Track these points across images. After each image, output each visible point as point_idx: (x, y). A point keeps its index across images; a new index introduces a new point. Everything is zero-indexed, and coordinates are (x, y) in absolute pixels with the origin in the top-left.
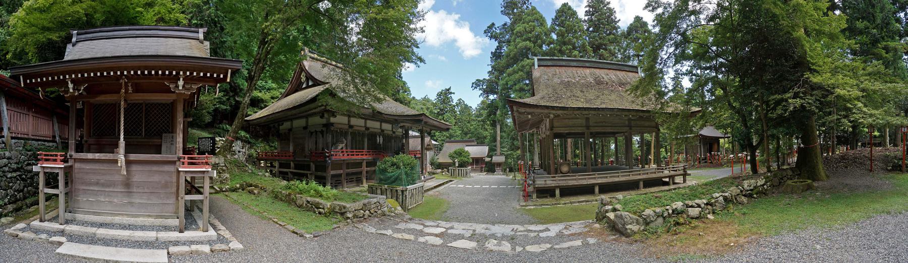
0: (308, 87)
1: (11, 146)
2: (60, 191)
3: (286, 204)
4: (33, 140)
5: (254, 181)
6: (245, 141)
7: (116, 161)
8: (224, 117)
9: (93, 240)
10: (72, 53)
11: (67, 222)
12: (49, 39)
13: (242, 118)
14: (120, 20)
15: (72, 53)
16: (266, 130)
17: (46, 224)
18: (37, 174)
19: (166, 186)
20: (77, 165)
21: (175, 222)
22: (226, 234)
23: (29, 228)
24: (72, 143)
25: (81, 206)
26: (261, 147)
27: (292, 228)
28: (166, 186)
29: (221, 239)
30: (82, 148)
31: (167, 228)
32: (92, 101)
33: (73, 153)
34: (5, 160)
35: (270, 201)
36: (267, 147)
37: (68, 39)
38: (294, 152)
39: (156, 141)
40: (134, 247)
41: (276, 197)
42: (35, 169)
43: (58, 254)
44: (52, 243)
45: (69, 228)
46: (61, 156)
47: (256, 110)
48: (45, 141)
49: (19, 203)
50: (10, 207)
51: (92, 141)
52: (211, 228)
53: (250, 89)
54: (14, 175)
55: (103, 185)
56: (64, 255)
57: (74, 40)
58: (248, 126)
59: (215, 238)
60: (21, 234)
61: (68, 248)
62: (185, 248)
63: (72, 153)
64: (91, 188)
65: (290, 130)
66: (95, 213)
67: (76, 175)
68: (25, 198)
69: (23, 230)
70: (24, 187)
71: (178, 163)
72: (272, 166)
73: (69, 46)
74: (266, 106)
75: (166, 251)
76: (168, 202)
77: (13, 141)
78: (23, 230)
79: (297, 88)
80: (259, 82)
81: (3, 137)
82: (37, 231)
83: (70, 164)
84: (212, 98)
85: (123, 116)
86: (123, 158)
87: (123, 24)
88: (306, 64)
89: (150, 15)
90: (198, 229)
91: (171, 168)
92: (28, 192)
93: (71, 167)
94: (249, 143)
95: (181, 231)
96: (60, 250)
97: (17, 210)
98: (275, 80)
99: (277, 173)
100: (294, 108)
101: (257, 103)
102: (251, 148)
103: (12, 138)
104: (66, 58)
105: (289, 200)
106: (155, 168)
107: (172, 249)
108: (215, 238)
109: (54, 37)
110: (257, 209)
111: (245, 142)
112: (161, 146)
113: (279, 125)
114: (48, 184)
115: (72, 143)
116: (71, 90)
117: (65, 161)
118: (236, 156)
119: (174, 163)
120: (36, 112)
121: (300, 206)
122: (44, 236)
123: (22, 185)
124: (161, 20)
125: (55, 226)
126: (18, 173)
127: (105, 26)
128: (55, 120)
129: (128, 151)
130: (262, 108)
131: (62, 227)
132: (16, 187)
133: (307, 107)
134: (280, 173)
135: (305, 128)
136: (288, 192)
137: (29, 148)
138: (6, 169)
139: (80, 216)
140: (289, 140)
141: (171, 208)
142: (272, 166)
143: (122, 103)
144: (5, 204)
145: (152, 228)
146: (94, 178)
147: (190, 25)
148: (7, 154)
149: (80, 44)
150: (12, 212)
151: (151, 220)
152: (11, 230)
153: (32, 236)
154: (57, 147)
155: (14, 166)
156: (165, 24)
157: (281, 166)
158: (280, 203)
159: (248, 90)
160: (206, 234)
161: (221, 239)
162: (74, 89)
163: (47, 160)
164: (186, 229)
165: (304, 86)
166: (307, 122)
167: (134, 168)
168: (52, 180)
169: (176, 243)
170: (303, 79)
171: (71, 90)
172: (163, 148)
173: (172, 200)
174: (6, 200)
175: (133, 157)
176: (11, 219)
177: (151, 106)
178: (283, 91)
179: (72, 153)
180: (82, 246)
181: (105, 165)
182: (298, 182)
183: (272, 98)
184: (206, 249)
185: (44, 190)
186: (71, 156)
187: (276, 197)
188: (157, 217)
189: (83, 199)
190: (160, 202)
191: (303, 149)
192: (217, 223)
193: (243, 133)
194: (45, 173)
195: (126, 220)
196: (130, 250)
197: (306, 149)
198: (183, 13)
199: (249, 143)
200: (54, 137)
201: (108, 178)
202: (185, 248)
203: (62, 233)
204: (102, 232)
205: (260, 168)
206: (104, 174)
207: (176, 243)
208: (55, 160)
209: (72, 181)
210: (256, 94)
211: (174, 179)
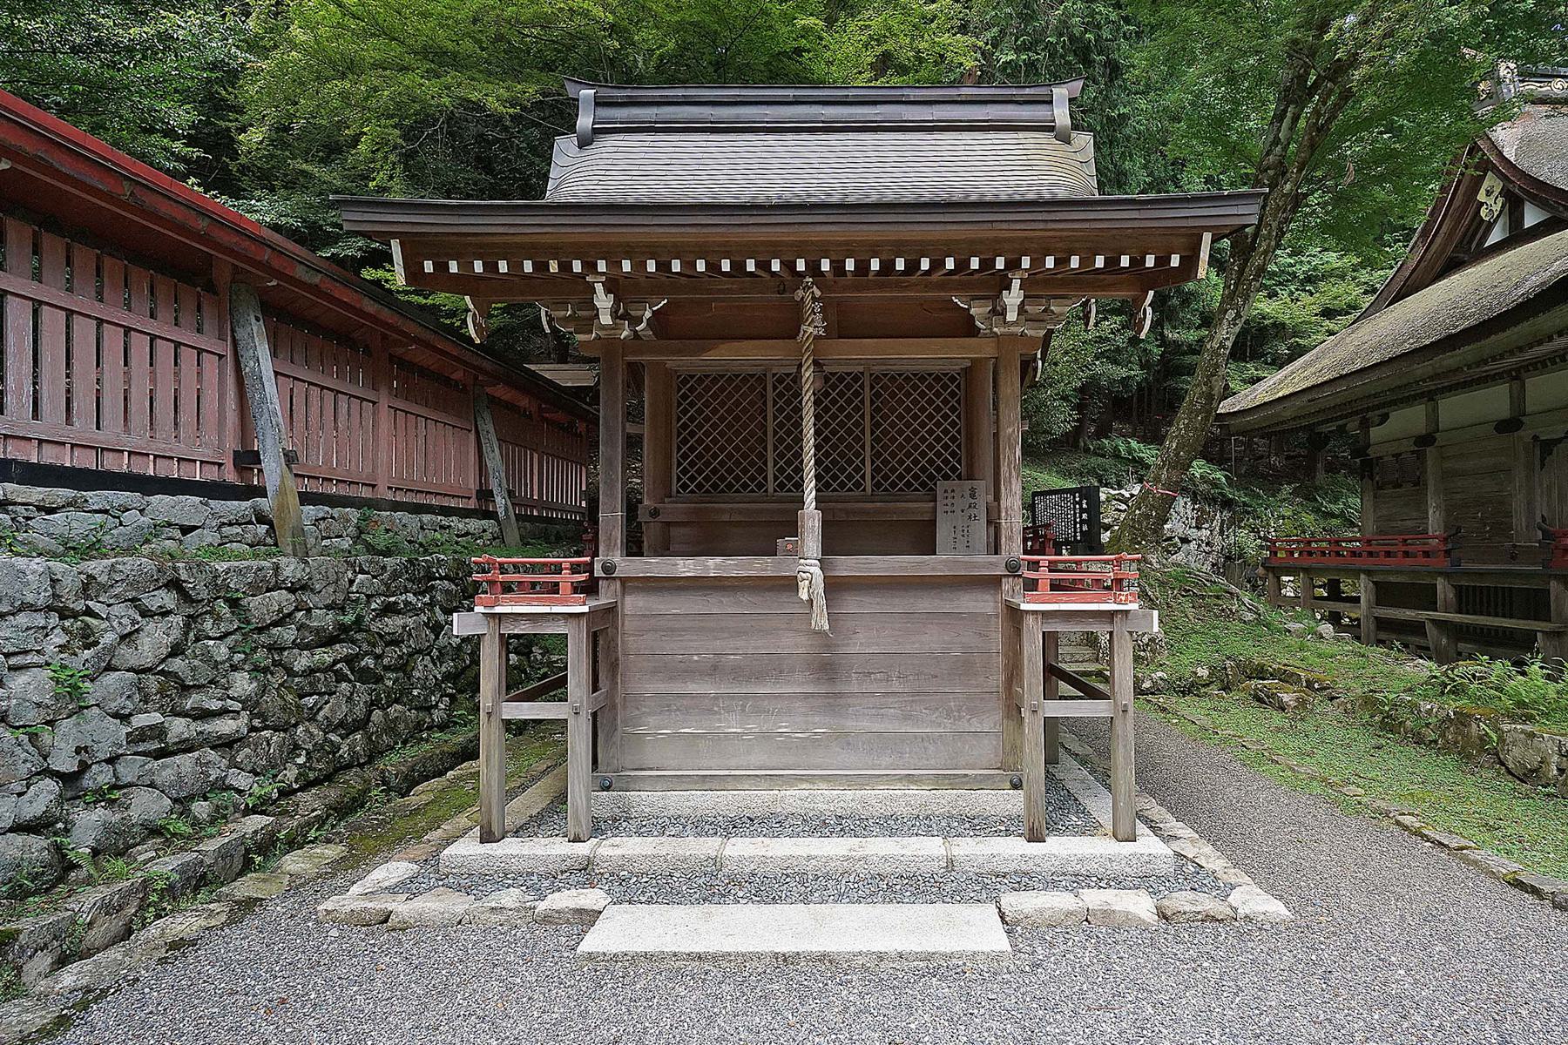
0: (1519, 235)
1: (299, 531)
2: (571, 709)
3: (1450, 760)
4: (396, 506)
6: (1209, 500)
7: (791, 584)
8: (1145, 403)
9: (715, 886)
10: (583, 171)
11: (598, 829)
12: (466, 103)
13: (1208, 409)
15: (583, 171)
16: (1307, 446)
17: (510, 847)
18: (473, 642)
19: (965, 667)
20: (633, 604)
21: (1012, 802)
22: (1213, 860)
23: (433, 874)
24: (612, 519)
25: (651, 757)
26: (1283, 518)
27: (1508, 866)
28: (965, 667)
29: (1188, 873)
31: (978, 825)
32: (673, 362)
33: (617, 558)
34: (280, 596)
35: (1365, 741)
36: (1308, 518)
37: (562, 116)
38: (1453, 535)
39: (916, 508)
40: (869, 898)
41: (1389, 725)
42: (461, 625)
43: (591, 957)
44: (547, 919)
45: (614, 849)
46: (575, 569)
48: (446, 511)
49: (352, 778)
50: (311, 802)
51: (675, 510)
52: (1141, 828)
53: (1237, 293)
54: (324, 656)
55: (737, 673)
56: (615, 958)
57: (585, 121)
58: (1227, 441)
59: (1167, 868)
60: (402, 908)
61: (624, 930)
62: (1060, 901)
63: (612, 555)
64: (692, 688)
65: (1425, 440)
66: (705, 782)
67: (632, 640)
68: (374, 754)
69: (407, 888)
70: (373, 704)
71: (1006, 585)
72: (1335, 593)
73: (565, 147)
74: (1297, 352)
75: (992, 909)
76: (975, 726)
77: (311, 511)
78: (407, 888)
79: (1463, 249)
80: (1284, 257)
81: (261, 492)
82: (474, 882)
83: (603, 600)
86: (816, 571)
88: (1507, 138)
89: (848, 45)
90: (1090, 828)
91: (983, 604)
92: (390, 727)
93: (611, 611)
94: (1227, 504)
95: (1035, 837)
96: (595, 941)
97: (343, 810)
98: (1337, 232)
99: (1367, 626)
100: (1449, 342)
101: (1261, 344)
102: (1235, 522)
103: (306, 498)
105: (1461, 742)
106: (925, 603)
107: (1010, 901)
108: (1167, 868)
109: (494, 97)
110: (1309, 767)
111: (1212, 500)
112: (933, 523)
113: (1365, 425)
114: (516, 684)
115: (612, 519)
116: (606, 319)
117: (589, 588)
118: (1179, 557)
119: (994, 582)
120: (406, 393)
121: (1529, 776)
122: (510, 898)
123: (362, 699)
125: (552, 848)
126: (343, 650)
128: (488, 427)
129: (831, 546)
130: (1279, 363)
131: (582, 849)
132: (334, 708)
133: (1524, 328)
134: (1383, 624)
135: (1508, 426)
136: (1452, 706)
137: (381, 541)
138: (288, 634)
139: (644, 800)
140: (1419, 483)
141: (987, 751)
142: (1335, 593)
143: (808, 373)
144: (285, 793)
146: (699, 649)
148: (291, 569)
149: (611, 141)
150: (321, 821)
152: (352, 899)
153: (459, 904)
154: (499, 537)
155: (324, 620)
156: (905, 84)
157: (1384, 593)
158: (1411, 750)
159: (1229, 298)
160: (1128, 848)
161: (1188, 873)
162: (614, 314)
163: (507, 588)
164: (1053, 827)
165: (1495, 237)
166: (1518, 399)
167: (853, 604)
168: (534, 666)
169: (1024, 880)
170: (1490, 201)
171: (606, 319)
172: (943, 533)
173: (990, 722)
174: (291, 773)
175: (849, 566)
176: (333, 852)
177: (891, 384)
178: (1379, 277)
179: (612, 555)
180: (679, 913)
181: (745, 598)
182: (1500, 668)
183: (1328, 313)
184: (1140, 905)
185: (497, 706)
186: (609, 569)
187: (1389, 722)
188: (941, 782)
189: (657, 731)
190: (947, 726)
191: (1502, 526)
192: (1156, 811)
193: (1199, 468)
194: (505, 640)
196: (862, 908)
197: (1519, 521)
198: (963, 29)
199: (1227, 504)
200: (485, 494)
201: (757, 645)
202: (1060, 901)
203: (586, 873)
204: (742, 849)
206: (739, 633)
207: (1024, 880)
208: (554, 588)
209: (614, 666)
210: (1263, 306)
211: (996, 640)
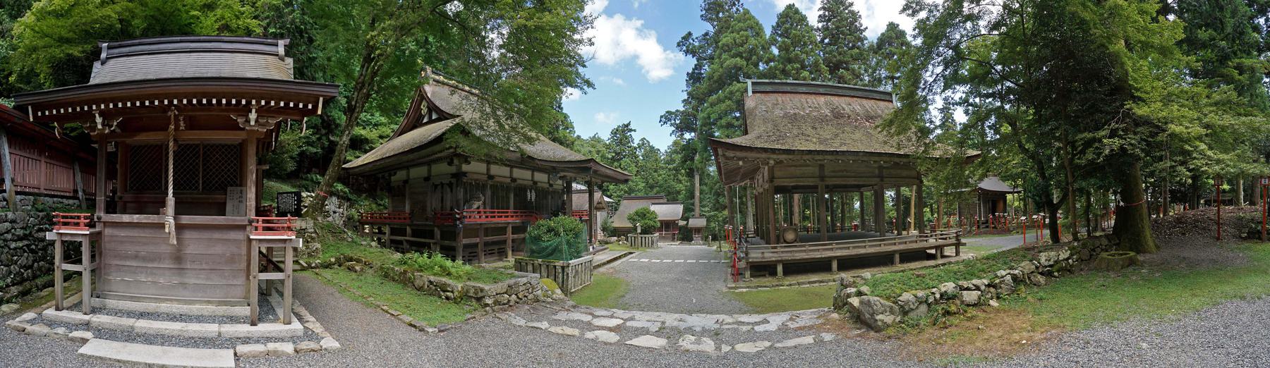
0: (431, 121)
1: (15, 204)
2: (85, 267)
3: (400, 286)
4: (46, 195)
5: (355, 253)
6: (343, 198)
7: (162, 226)
8: (313, 164)
9: (130, 336)
10: (101, 74)
11: (94, 311)
12: (68, 55)
13: (339, 166)
14: (168, 28)
15: (101, 74)
16: (372, 182)
17: (64, 314)
18: (52, 243)
19: (232, 260)
20: (108, 231)
21: (245, 311)
22: (317, 327)
23: (40, 319)
24: (101, 200)
25: (114, 288)
26: (365, 206)
27: (408, 319)
28: (232, 260)
29: (309, 335)
30: (115, 207)
31: (233, 320)
32: (128, 141)
33: (102, 214)
34: (7, 225)
35: (378, 281)
36: (374, 206)
37: (96, 55)
38: (412, 213)
39: (218, 197)
40: (187, 346)
41: (386, 276)
42: (49, 236)
43: (82, 355)
44: (73, 340)
45: (97, 319)
46: (86, 218)
47: (357, 153)
48: (62, 197)
49: (27, 284)
50: (14, 290)
51: (128, 197)
52: (295, 319)
53: (350, 125)
54: (20, 244)
55: (144, 259)
56: (90, 357)
57: (103, 55)
58: (346, 177)
59: (301, 333)
60: (29, 328)
61: (96, 348)
62: (259, 348)
63: (100, 213)
64: (128, 263)
65: (406, 182)
66: (132, 299)
67: (107, 245)
68: (35, 277)
69: (32, 322)
70: (34, 261)
71: (248, 228)
72: (380, 232)
73: (97, 65)
74: (372, 149)
75: (232, 351)
76: (235, 282)
77: (19, 197)
78: (32, 322)
79: (416, 123)
80: (362, 115)
81: (5, 191)
82: (51, 323)
83: (97, 229)
84: (297, 137)
85: (172, 162)
86: (172, 221)
87: (172, 34)
88: (428, 89)
90: (276, 320)
91: (239, 235)
92: (40, 269)
93: (99, 233)
94: (349, 200)
95: (253, 324)
96: (84, 350)
97: (24, 294)
98: (384, 112)
99: (388, 243)
100: (412, 151)
101: (359, 145)
102: (351, 206)
103: (17, 193)
104: (93, 81)
105: (404, 280)
106: (217, 235)
107: (241, 349)
108: (301, 333)
109: (76, 51)
110: (360, 292)
111: (343, 198)
112: (225, 204)
113: (390, 175)
114: (67, 258)
115: (101, 200)
116: (100, 127)
117: (91, 225)
118: (330, 219)
119: (243, 228)
120: (50, 157)
121: (420, 289)
122: (61, 330)
123: (31, 259)
124: (226, 27)
125: (78, 316)
126: (26, 242)
127: (147, 37)
128: (77, 168)
129: (178, 212)
130: (366, 152)
131: (87, 317)
132: (23, 261)
133: (429, 150)
134: (392, 241)
135: (427, 179)
136: (403, 268)
137: (41, 207)
138: (9, 236)
139: (111, 303)
140: (404, 196)
141: (239, 292)
142: (380, 232)
143: (171, 144)
144: (8, 286)
145: (212, 319)
146: (131, 249)
147: (265, 36)
148: (10, 215)
149: (112, 62)
150: (16, 297)
151: (211, 308)
152: (15, 322)
153: (45, 330)
154: (80, 206)
155: (20, 232)
157: (393, 232)
158: (392, 283)
159: (347, 126)
160: (288, 327)
161: (309, 335)
162: (103, 125)
163: (65, 224)
164: (260, 320)
165: (425, 120)
166: (429, 171)
167: (188, 235)
168: (72, 252)
169: (247, 340)
170: (424, 110)
171: (100, 127)
172: (229, 208)
173: (241, 280)
174: (9, 280)
175: (186, 219)
176: (15, 306)
177: (211, 148)
178: (395, 127)
179: (100, 213)
180: (115, 344)
181: (147, 231)
182: (417, 255)
183: (381, 137)
184: (288, 348)
185: (62, 267)
186: (99, 218)
187: (386, 275)
188: (220, 303)
189: (115, 279)
190: (224, 282)
191: (424, 209)
192: (303, 312)
193: (340, 187)
194: (63, 242)
195: (176, 308)
196: (182, 349)
197: (429, 209)
198: (256, 18)
199: (349, 200)
200: (76, 191)
201: (151, 248)
202: (259, 348)
203: (87, 326)
204: (142, 324)
205: (363, 235)
206: (145, 244)
207: (247, 340)
208: (77, 224)
209: (101, 254)
210: (359, 131)
211: (244, 251)
